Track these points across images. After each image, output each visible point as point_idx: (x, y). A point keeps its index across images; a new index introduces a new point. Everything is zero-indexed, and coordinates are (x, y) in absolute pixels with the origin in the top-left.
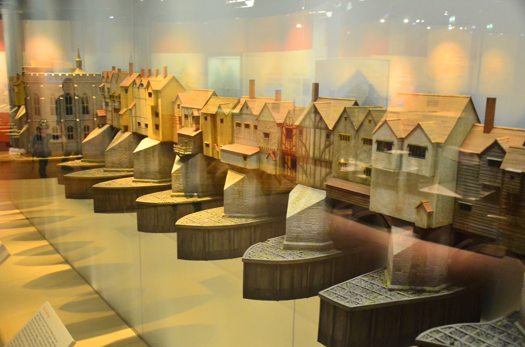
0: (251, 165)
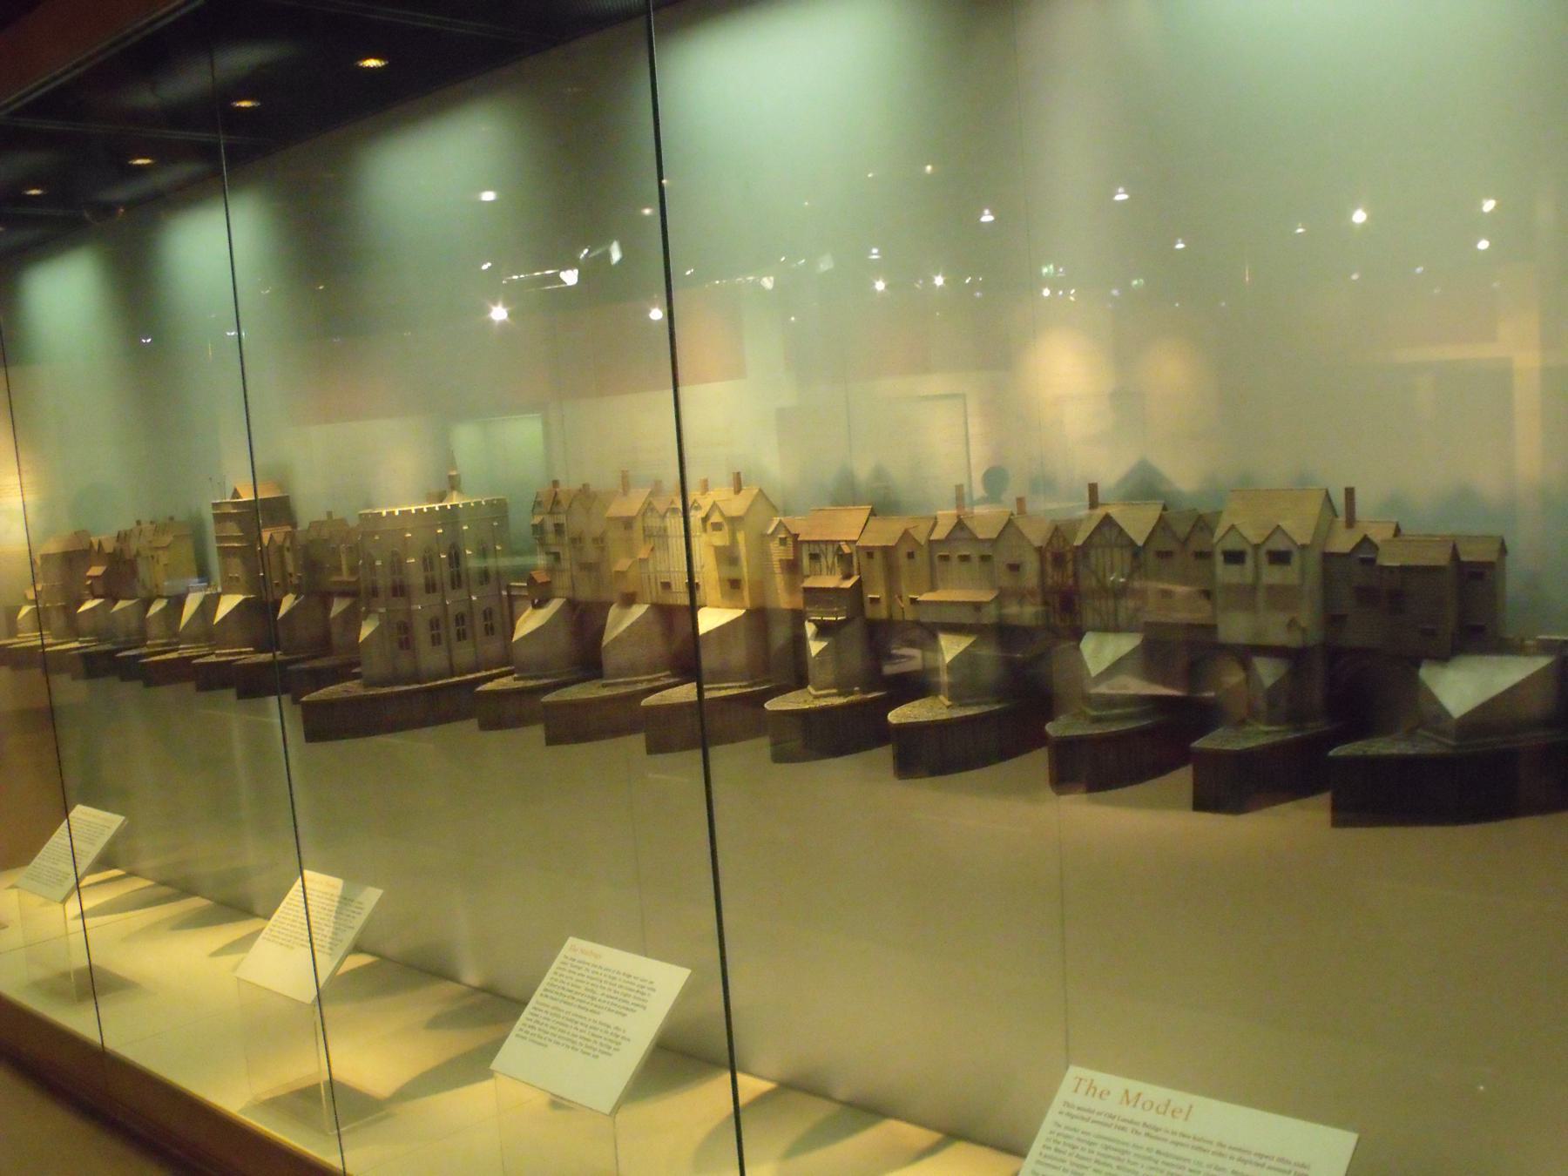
0: (989, 616)
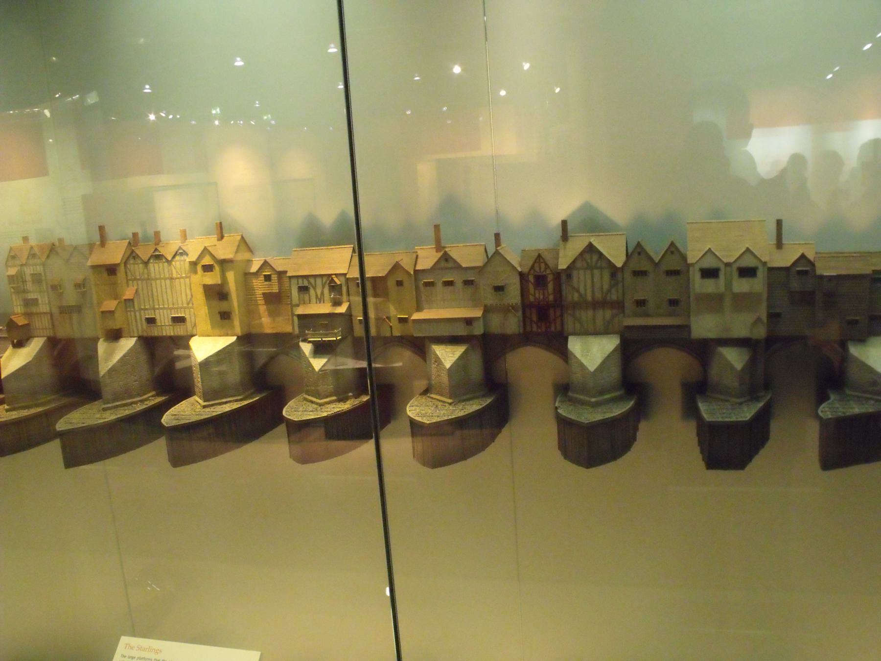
0: (478, 330)
